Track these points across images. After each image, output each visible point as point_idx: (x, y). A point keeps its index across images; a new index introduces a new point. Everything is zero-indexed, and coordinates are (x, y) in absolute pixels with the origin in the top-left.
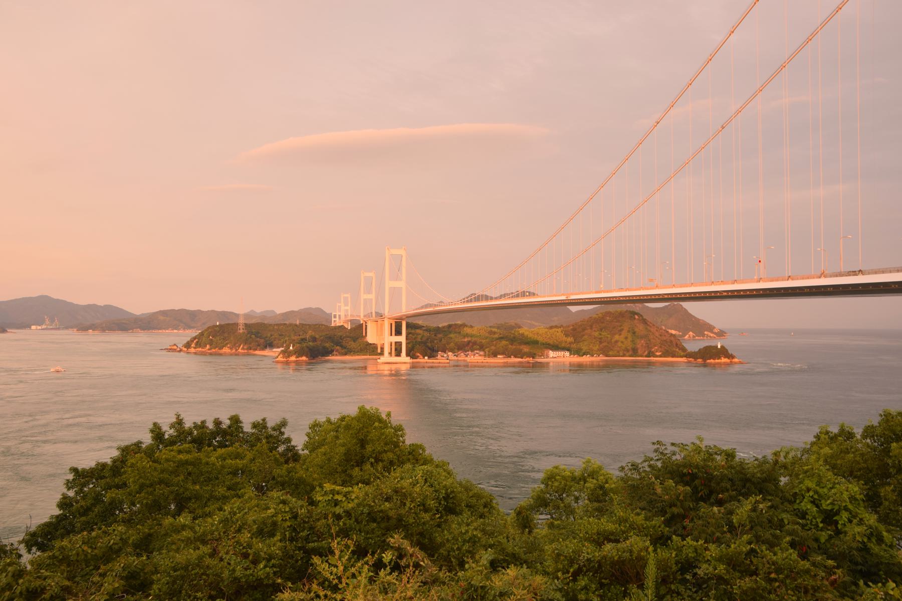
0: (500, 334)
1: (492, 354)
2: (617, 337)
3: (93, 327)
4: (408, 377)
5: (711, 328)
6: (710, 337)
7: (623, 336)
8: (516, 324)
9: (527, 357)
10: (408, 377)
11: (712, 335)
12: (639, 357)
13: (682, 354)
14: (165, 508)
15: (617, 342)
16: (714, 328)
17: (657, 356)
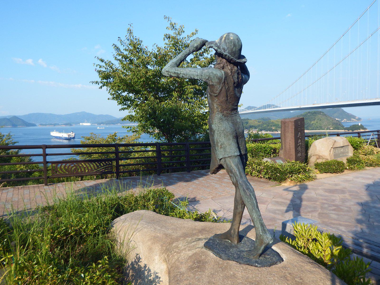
0: (263, 122)
1: (260, 130)
2: (313, 122)
3: (103, 123)
4: (17, 228)
5: (354, 117)
6: (354, 121)
7: (315, 121)
8: (268, 118)
9: (275, 131)
10: (17, 228)
11: (355, 120)
12: (322, 130)
13: (341, 128)
14: (58, 239)
15: (313, 124)
16: (356, 117)
17: (331, 130)
